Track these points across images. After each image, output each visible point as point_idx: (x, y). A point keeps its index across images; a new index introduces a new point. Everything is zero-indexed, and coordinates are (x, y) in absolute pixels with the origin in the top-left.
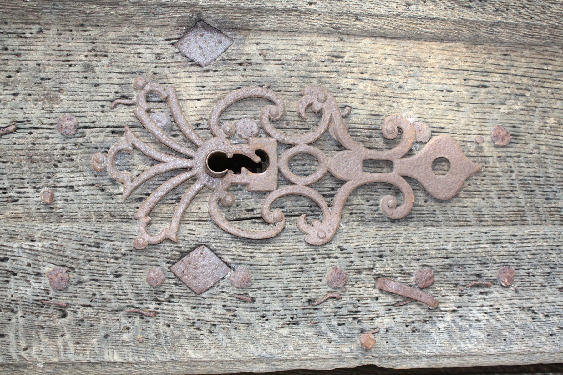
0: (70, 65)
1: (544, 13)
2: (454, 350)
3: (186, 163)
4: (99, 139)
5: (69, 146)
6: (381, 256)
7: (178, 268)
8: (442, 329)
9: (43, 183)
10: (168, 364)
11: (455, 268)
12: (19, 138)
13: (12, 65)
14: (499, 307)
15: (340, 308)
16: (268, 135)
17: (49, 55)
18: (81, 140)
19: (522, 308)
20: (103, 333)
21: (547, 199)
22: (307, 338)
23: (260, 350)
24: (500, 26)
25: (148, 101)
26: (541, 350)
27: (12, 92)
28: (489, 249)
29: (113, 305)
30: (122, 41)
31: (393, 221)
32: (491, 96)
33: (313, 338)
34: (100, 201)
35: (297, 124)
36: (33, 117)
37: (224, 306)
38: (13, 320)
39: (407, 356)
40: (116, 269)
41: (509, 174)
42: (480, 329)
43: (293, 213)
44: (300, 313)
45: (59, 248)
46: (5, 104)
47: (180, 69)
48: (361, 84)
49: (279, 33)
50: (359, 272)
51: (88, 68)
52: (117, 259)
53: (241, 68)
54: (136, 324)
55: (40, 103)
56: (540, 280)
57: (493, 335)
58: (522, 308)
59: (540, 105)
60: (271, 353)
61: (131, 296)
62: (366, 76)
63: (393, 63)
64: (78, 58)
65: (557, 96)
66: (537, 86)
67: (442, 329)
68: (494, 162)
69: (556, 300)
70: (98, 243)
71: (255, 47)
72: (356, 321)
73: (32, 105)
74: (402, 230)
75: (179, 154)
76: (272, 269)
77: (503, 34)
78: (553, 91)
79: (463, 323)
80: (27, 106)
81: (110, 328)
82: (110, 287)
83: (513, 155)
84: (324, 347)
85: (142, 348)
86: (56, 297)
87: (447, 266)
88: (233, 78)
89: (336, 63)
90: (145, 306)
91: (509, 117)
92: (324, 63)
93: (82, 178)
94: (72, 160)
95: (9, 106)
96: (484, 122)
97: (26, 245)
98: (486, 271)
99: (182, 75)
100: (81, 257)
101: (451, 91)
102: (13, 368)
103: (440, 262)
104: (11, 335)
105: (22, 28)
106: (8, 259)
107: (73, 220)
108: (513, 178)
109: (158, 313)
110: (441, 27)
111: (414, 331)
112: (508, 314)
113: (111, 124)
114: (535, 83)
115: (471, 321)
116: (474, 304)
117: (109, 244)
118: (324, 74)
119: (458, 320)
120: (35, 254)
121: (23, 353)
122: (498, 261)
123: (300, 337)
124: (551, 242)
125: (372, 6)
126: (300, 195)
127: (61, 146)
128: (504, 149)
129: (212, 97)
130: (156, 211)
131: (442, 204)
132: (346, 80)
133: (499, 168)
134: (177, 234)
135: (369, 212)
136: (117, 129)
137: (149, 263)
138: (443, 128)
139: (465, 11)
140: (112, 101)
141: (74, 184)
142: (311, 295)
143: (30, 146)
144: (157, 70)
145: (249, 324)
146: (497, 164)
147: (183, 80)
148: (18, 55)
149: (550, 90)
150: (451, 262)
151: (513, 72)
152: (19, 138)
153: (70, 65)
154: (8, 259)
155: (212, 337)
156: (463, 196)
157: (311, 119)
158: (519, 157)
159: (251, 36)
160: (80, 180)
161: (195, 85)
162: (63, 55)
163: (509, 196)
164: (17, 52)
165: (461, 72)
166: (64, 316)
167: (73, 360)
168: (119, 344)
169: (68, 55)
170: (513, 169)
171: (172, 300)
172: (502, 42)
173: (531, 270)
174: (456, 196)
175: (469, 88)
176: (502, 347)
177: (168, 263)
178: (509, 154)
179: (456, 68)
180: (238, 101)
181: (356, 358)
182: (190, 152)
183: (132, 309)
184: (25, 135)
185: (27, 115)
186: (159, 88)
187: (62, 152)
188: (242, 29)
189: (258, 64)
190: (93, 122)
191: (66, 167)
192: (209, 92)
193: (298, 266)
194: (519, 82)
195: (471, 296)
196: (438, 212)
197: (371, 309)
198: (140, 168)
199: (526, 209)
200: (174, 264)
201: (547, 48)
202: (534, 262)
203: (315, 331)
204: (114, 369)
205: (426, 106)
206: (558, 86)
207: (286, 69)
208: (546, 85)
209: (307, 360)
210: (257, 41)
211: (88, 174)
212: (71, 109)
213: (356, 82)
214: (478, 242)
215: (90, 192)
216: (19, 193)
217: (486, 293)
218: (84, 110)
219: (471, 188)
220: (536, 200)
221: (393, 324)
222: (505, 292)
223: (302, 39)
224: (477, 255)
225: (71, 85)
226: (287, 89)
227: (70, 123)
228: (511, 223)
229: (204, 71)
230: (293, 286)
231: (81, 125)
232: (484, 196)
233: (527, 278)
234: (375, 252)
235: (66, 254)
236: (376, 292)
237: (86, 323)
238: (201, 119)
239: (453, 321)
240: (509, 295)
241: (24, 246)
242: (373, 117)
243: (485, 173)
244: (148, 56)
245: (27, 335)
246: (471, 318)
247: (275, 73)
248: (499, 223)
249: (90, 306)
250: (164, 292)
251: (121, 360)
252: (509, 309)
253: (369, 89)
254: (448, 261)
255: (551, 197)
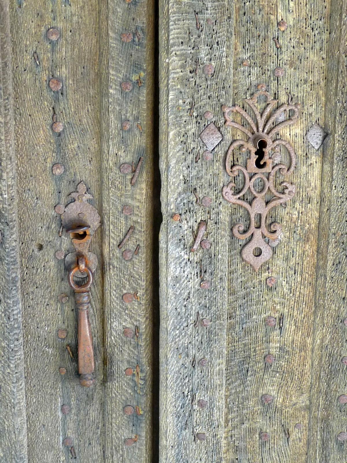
0: (307, 73)
1: (331, 301)
2: (170, 260)
3: (261, 129)
4: (272, 87)
5: (269, 73)
6: (216, 223)
7: (212, 126)
8: (181, 254)
9: (252, 61)
10: (167, 121)
11: (210, 260)
12: (273, 49)
13: (307, 45)
14: (191, 282)
15: (192, 204)
16: (273, 168)
17: (312, 63)
18: (272, 78)
19: (189, 294)
20: (183, 91)
21: (240, 306)
22: (178, 188)
23: (173, 165)
24: (325, 279)
25: (290, 110)
26: (169, 303)
27: (295, 45)
28: (218, 276)
29: (196, 95)
30: (318, 98)
31: (232, 230)
32: (290, 277)
33: (178, 191)
34: (243, 88)
35: (278, 182)
36: (283, 56)
37: (194, 148)
38: (189, 48)
39: (168, 236)
40: (212, 97)
41: (253, 286)
42: (180, 273)
43: (236, 180)
44: (190, 184)
45: (223, 69)
46: (289, 42)
47: (304, 126)
48: (297, 212)
49: (321, 172)
50: (209, 213)
51: (306, 81)
52: (217, 97)
53: (305, 154)
54: (186, 106)
55: (290, 59)
56: (203, 302)
57: (177, 279)
58: (189, 294)
59: (286, 301)
60: (171, 170)
61: (200, 104)
62: (300, 214)
63: (306, 228)
64: (310, 76)
65: (290, 310)
66: (295, 299)
67: (181, 254)
68: (259, 278)
69: (193, 310)
70: (224, 88)
71: (315, 160)
72: (185, 211)
73: (288, 55)
74: (227, 233)
75: (265, 126)
76: (211, 171)
77: (320, 281)
78: (293, 308)
79: (183, 264)
80: (288, 53)
81: (185, 94)
82: (204, 94)
83: (262, 288)
84: (174, 196)
85: (175, 109)
86: (200, 68)
87: (210, 256)
88: (300, 151)
89: (306, 200)
90: (195, 110)
91: (280, 285)
92: (306, 194)
93: (254, 79)
94: (263, 74)
95: (288, 44)
96: (278, 274)
97: (224, 54)
98: (208, 275)
99: (302, 126)
100: (218, 80)
101: (293, 257)
102: (166, 48)
103: (213, 252)
104: (183, 47)
105: (324, 50)
106: (218, 45)
107: (234, 75)
108: (251, 288)
109: (191, 117)
110: (324, 250)
111: (180, 240)
112: (187, 286)
113: (279, 92)
114: (296, 298)
115: (184, 268)
116: (192, 269)
117: (224, 93)
118: (301, 195)
119: (185, 262)
120: (220, 58)
121: (174, 53)
122: (213, 281)
123: (179, 184)
124: (221, 307)
125: (334, 217)
126: (244, 183)
127: (269, 69)
128: (265, 284)
129: (291, 140)
130: (238, 115)
131: (239, 254)
132: (298, 205)
133: (256, 281)
134: (229, 125)
135: (236, 218)
136: (277, 95)
137: (215, 112)
138: (275, 253)
139: (332, 262)
140: (290, 93)
141: (251, 75)
142: (198, 189)
143: (270, 54)
144: (304, 114)
145: (185, 160)
146: (258, 280)
147: (299, 127)
148: (312, 48)
149: (293, 306)
150: (212, 257)
151: (302, 287)
152: (273, 49)
153: (307, 73)
154: (218, 45)
155: (180, 142)
156: (243, 263)
157: (280, 188)
158: (261, 291)
159: (320, 159)
160: (253, 78)
161: (297, 132)
162: (312, 69)
163: (242, 286)
164: (314, 48)
165: (302, 261)
166: (190, 72)
167: (170, 77)
168: (177, 98)
169: (312, 72)
170: (255, 288)
171: (197, 123)
172: (316, 281)
173: (207, 297)
174: (243, 260)
175: (294, 265)
176: (171, 284)
177: (215, 121)
178: (262, 286)
179: (304, 259)
180: (289, 153)
181: (167, 212)
182: (265, 131)
183: (193, 104)
184: (275, 52)
185: (284, 53)
186: (296, 116)
187: (266, 69)
188: (324, 155)
189: (306, 162)
190: (280, 84)
191: (259, 71)
192: (294, 139)
193: (212, 183)
194: (297, 290)
195: (196, 268)
196: (235, 251)
197: (191, 218)
198: (258, 106)
199: (236, 295)
200: (214, 124)
201: (314, 304)
202: (211, 299)
203: (181, 191)
204: (164, 96)
205: (286, 244)
206: (295, 310)
207: (304, 176)
208: (296, 303)
209: (167, 188)
210: (317, 162)
211: (256, 82)
212: (286, 74)
213: (298, 210)
214: (222, 271)
215: (247, 83)
216: (248, 49)
217: (197, 276)
218: (286, 79)
219: (246, 267)
220: (240, 300)
221: (184, 229)
222: (197, 285)
223: (318, 183)
224: (216, 270)
225: (298, 74)
226: (295, 176)
227: (280, 74)
228: (229, 288)
229: (303, 137)
230: (203, 180)
231: (279, 78)
232: (242, 274)
233: (204, 295)
234: (218, 220)
235: (220, 73)
236: (199, 221)
237: (188, 83)
238: (281, 136)
239: (184, 259)
240: (196, 286)
241: (224, 53)
242: (281, 218)
243: (253, 274)
244: (311, 110)
245: (182, 55)
246: (185, 268)
247: (302, 171)
248: (229, 282)
249: (195, 84)
250: (201, 119)
251: (169, 99)
252: (189, 287)
253: (294, 216)
254: (213, 256)
255: (241, 308)
